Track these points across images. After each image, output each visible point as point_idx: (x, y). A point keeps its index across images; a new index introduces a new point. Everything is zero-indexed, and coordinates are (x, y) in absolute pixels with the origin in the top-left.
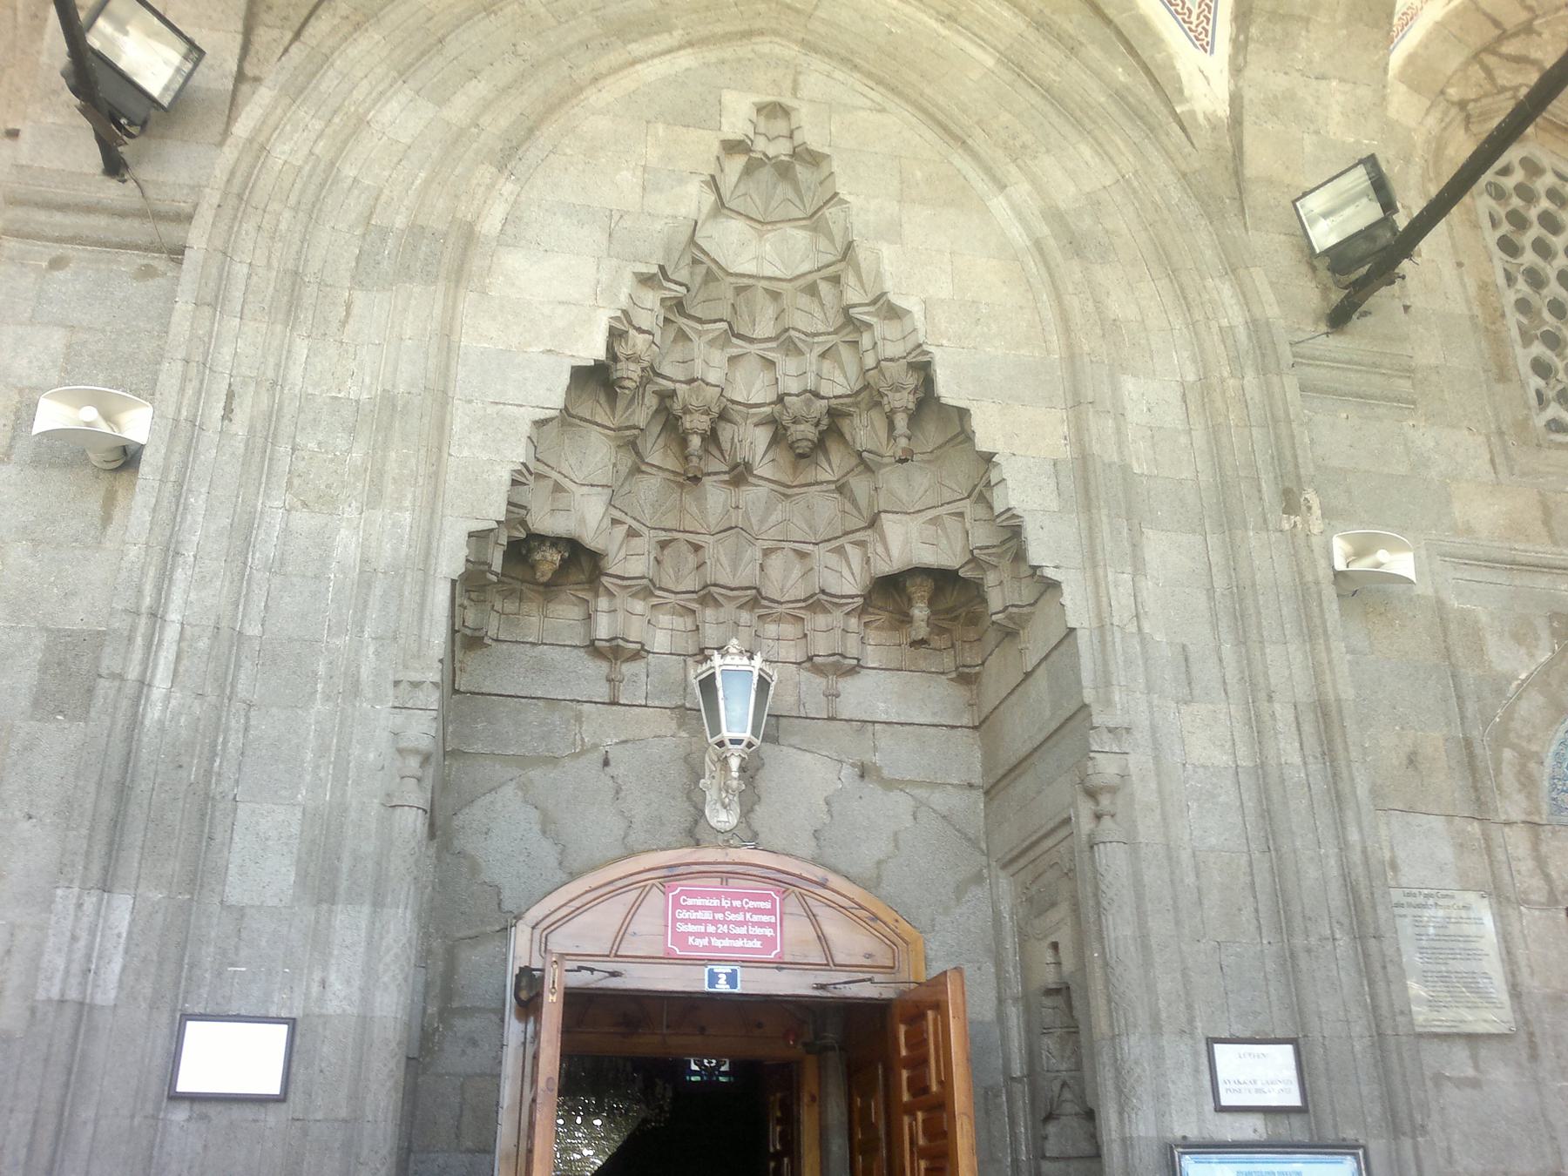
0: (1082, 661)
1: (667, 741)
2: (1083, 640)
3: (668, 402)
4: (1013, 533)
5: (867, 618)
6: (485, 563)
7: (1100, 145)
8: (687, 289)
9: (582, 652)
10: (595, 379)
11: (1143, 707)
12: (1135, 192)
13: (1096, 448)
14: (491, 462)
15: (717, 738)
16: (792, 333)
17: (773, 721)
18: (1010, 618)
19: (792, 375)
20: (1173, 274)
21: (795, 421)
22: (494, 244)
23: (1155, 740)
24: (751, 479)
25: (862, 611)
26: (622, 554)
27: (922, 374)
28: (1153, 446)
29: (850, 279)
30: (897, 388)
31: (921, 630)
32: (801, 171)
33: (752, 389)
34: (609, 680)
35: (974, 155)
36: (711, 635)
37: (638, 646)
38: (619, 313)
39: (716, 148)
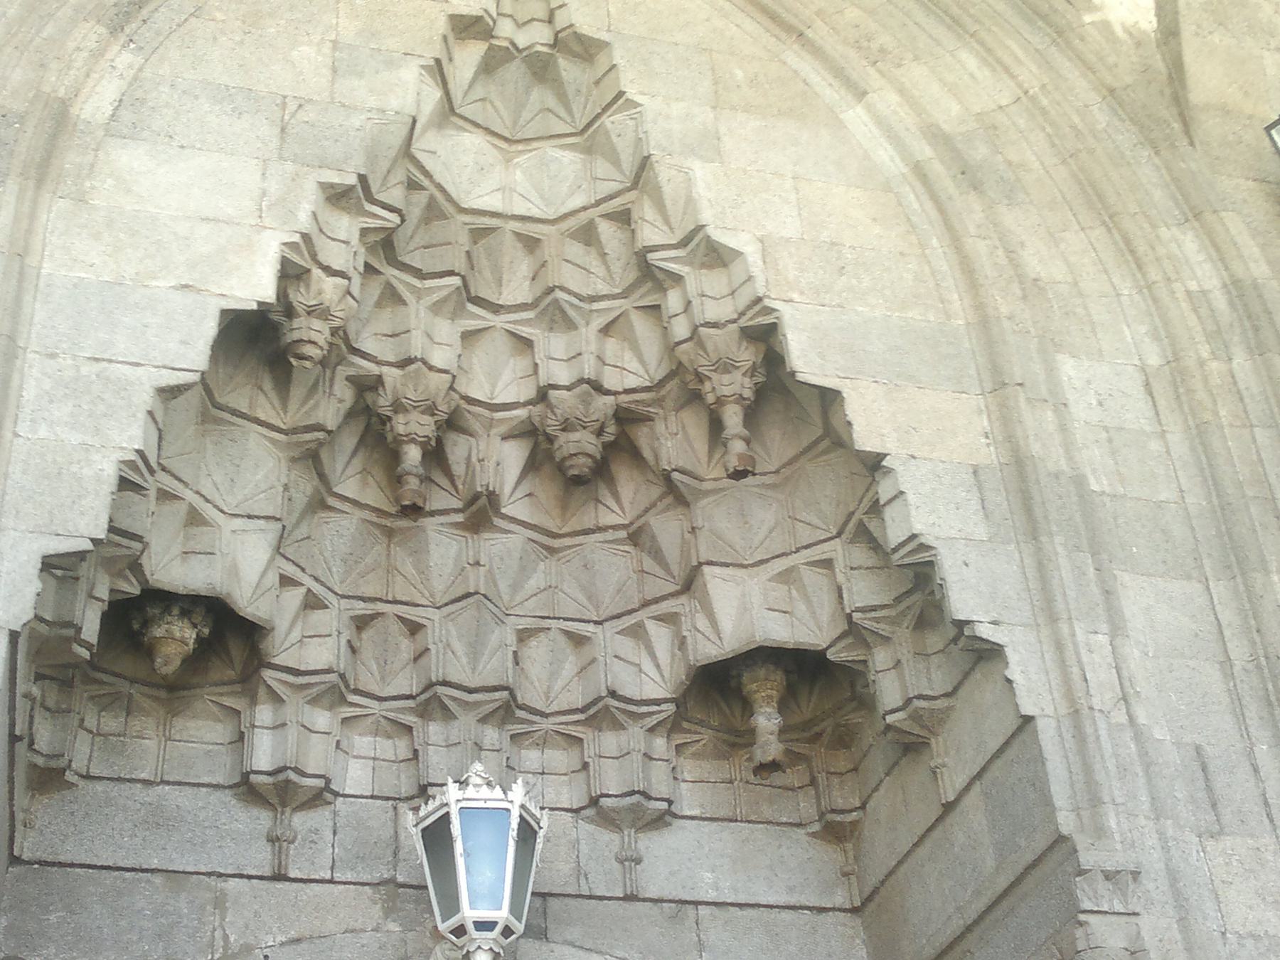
0: (1050, 766)
1: (365, 938)
2: (1047, 731)
3: (369, 397)
4: (919, 578)
5: (679, 739)
6: (69, 624)
7: (989, 50)
8: (394, 218)
9: (227, 796)
10: (255, 339)
11: (1152, 841)
12: (1044, 112)
13: (1035, 448)
14: (86, 447)
15: (453, 922)
16: (560, 294)
17: (538, 902)
18: (916, 717)
19: (559, 359)
20: (1110, 219)
21: (567, 427)
22: (101, 133)
23: (1177, 894)
24: (497, 521)
25: (673, 726)
26: (296, 635)
27: (762, 347)
28: (1114, 453)
29: (646, 211)
30: (726, 366)
31: (769, 746)
32: (567, 69)
33: (498, 380)
34: (273, 840)
35: (816, 51)
36: (436, 761)
37: (320, 783)
38: (296, 238)
39: (442, 25)
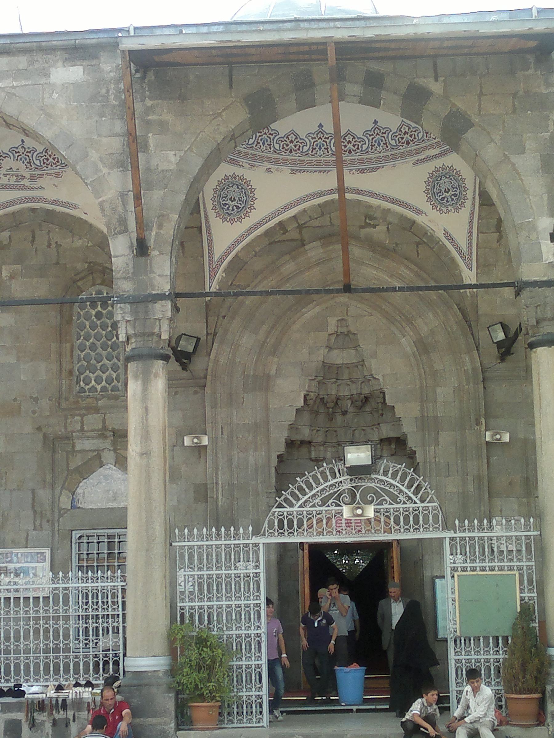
33: (345, 392)
